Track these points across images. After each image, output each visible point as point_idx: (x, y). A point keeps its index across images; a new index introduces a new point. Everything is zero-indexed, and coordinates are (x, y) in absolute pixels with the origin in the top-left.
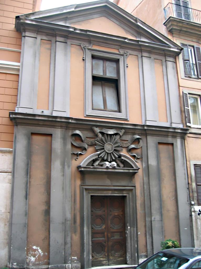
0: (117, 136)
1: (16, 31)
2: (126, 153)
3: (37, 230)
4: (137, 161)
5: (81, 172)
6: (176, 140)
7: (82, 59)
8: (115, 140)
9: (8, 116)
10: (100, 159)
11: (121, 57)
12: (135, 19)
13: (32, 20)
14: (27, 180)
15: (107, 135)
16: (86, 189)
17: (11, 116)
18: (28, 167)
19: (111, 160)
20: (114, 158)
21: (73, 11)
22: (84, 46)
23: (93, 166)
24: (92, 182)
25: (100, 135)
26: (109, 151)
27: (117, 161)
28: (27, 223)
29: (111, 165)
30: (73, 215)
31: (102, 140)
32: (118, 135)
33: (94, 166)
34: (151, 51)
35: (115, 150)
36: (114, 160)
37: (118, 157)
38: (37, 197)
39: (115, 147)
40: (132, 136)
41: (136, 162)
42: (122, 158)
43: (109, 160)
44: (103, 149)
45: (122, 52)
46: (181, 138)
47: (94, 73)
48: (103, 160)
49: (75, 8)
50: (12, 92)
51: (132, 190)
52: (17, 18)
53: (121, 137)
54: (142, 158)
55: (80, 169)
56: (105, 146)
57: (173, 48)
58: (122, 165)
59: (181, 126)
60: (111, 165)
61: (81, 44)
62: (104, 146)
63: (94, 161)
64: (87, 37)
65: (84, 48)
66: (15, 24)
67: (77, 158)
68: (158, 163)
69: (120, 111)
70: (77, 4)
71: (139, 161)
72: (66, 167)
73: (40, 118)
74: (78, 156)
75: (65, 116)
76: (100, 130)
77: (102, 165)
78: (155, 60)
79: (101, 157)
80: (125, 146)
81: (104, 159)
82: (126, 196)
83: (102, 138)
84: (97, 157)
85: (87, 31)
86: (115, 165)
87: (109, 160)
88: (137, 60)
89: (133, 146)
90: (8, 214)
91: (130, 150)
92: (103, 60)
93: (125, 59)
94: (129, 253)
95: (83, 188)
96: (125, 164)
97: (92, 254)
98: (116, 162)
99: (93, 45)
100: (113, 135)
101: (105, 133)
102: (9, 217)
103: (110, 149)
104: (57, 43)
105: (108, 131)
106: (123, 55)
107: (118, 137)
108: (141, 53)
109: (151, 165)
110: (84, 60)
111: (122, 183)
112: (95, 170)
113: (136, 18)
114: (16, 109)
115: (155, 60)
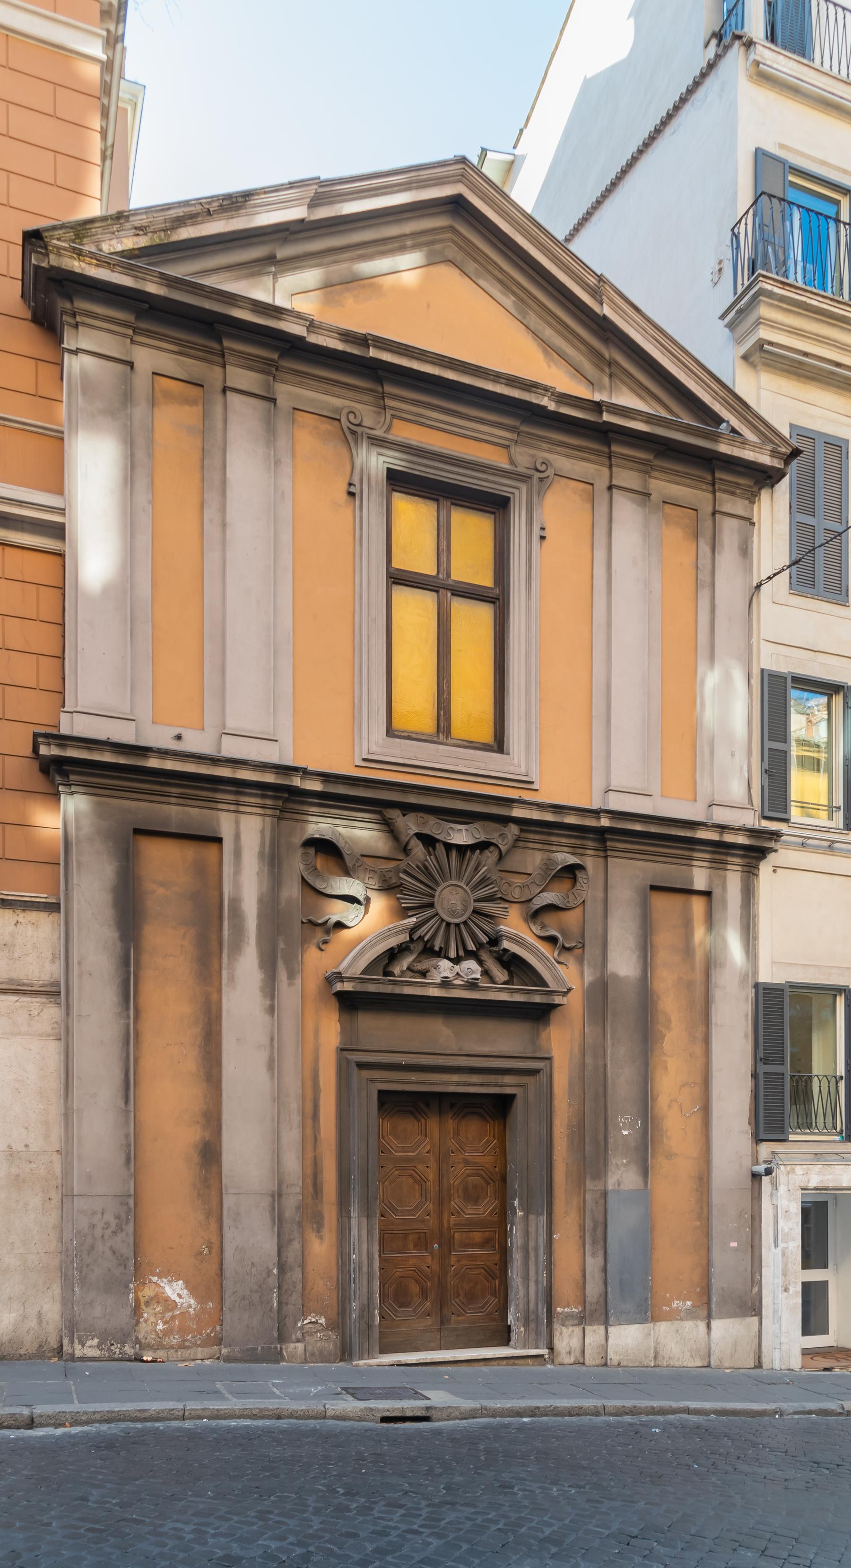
0: (487, 853)
1: (30, 317)
2: (522, 925)
3: (173, 1216)
4: (561, 959)
5: (341, 997)
6: (725, 877)
7: (343, 487)
8: (477, 869)
9: (28, 751)
10: (419, 947)
11: (518, 488)
12: (592, 281)
13: (102, 261)
14: (128, 1026)
15: (449, 847)
16: (361, 1066)
17: (43, 750)
18: (129, 973)
19: (461, 953)
20: (471, 946)
21: (302, 221)
22: (357, 422)
23: (387, 973)
24: (385, 1033)
25: (418, 849)
26: (453, 916)
27: (484, 956)
28: (132, 1192)
29: (458, 974)
30: (309, 1162)
31: (426, 868)
32: (492, 848)
33: (392, 974)
34: (662, 451)
35: (476, 912)
36: (472, 951)
37: (488, 943)
38: (170, 1096)
39: (475, 901)
40: (545, 855)
41: (559, 963)
42: (506, 944)
43: (452, 954)
44: (431, 905)
45: (523, 457)
46: (746, 869)
47: (395, 564)
48: (430, 951)
49: (314, 204)
50: (41, 638)
51: (536, 1070)
52: (33, 239)
53: (501, 857)
54: (583, 946)
55: (339, 987)
56: (437, 894)
57: (754, 447)
58: (500, 975)
59: (750, 819)
60: (458, 974)
61: (338, 410)
62: (433, 896)
63: (393, 955)
64: (370, 370)
65: (353, 433)
66: (23, 280)
67: (325, 942)
68: (645, 971)
69: (499, 744)
70: (325, 175)
71: (570, 959)
72: (282, 975)
73: (170, 765)
74: (328, 932)
75: (275, 759)
76: (418, 826)
77: (424, 974)
78: (668, 509)
79: (421, 938)
80: (516, 894)
81: (434, 946)
82: (512, 1097)
83: (426, 860)
84: (404, 937)
85: (364, 341)
86: (473, 972)
87: (452, 954)
88: (589, 506)
89: (549, 897)
90: (56, 1158)
91: (535, 915)
92: (437, 500)
93: (535, 499)
94: (517, 1306)
95: (348, 1061)
96: (514, 965)
97: (381, 1308)
98: (480, 962)
99: (393, 416)
100: (472, 848)
101: (438, 841)
102: (58, 1171)
103: (459, 907)
104: (231, 396)
105: (450, 831)
106: (524, 478)
107: (490, 857)
108: (606, 471)
109: (615, 976)
110: (351, 494)
111: (503, 1040)
112: (397, 990)
113: (600, 278)
114: (64, 718)
115: (667, 506)
